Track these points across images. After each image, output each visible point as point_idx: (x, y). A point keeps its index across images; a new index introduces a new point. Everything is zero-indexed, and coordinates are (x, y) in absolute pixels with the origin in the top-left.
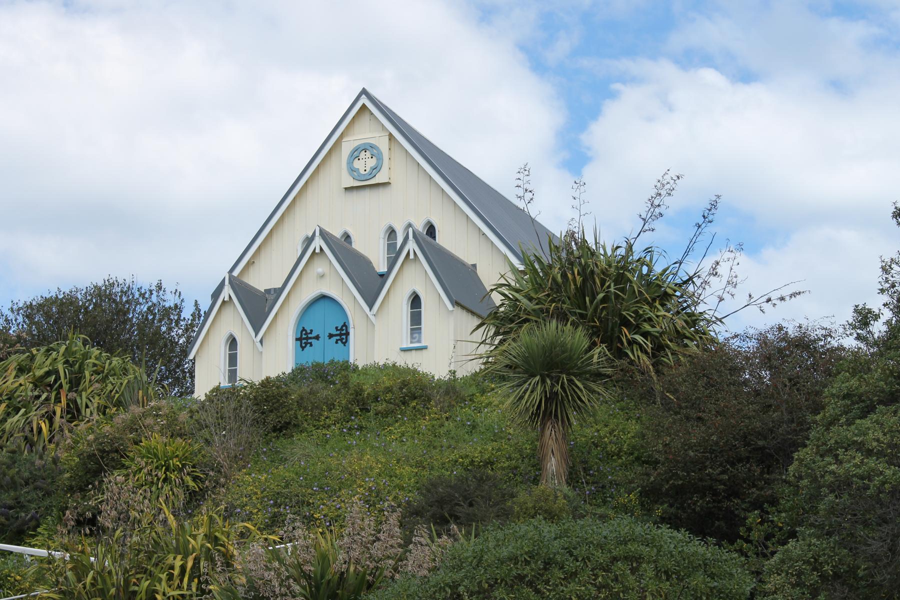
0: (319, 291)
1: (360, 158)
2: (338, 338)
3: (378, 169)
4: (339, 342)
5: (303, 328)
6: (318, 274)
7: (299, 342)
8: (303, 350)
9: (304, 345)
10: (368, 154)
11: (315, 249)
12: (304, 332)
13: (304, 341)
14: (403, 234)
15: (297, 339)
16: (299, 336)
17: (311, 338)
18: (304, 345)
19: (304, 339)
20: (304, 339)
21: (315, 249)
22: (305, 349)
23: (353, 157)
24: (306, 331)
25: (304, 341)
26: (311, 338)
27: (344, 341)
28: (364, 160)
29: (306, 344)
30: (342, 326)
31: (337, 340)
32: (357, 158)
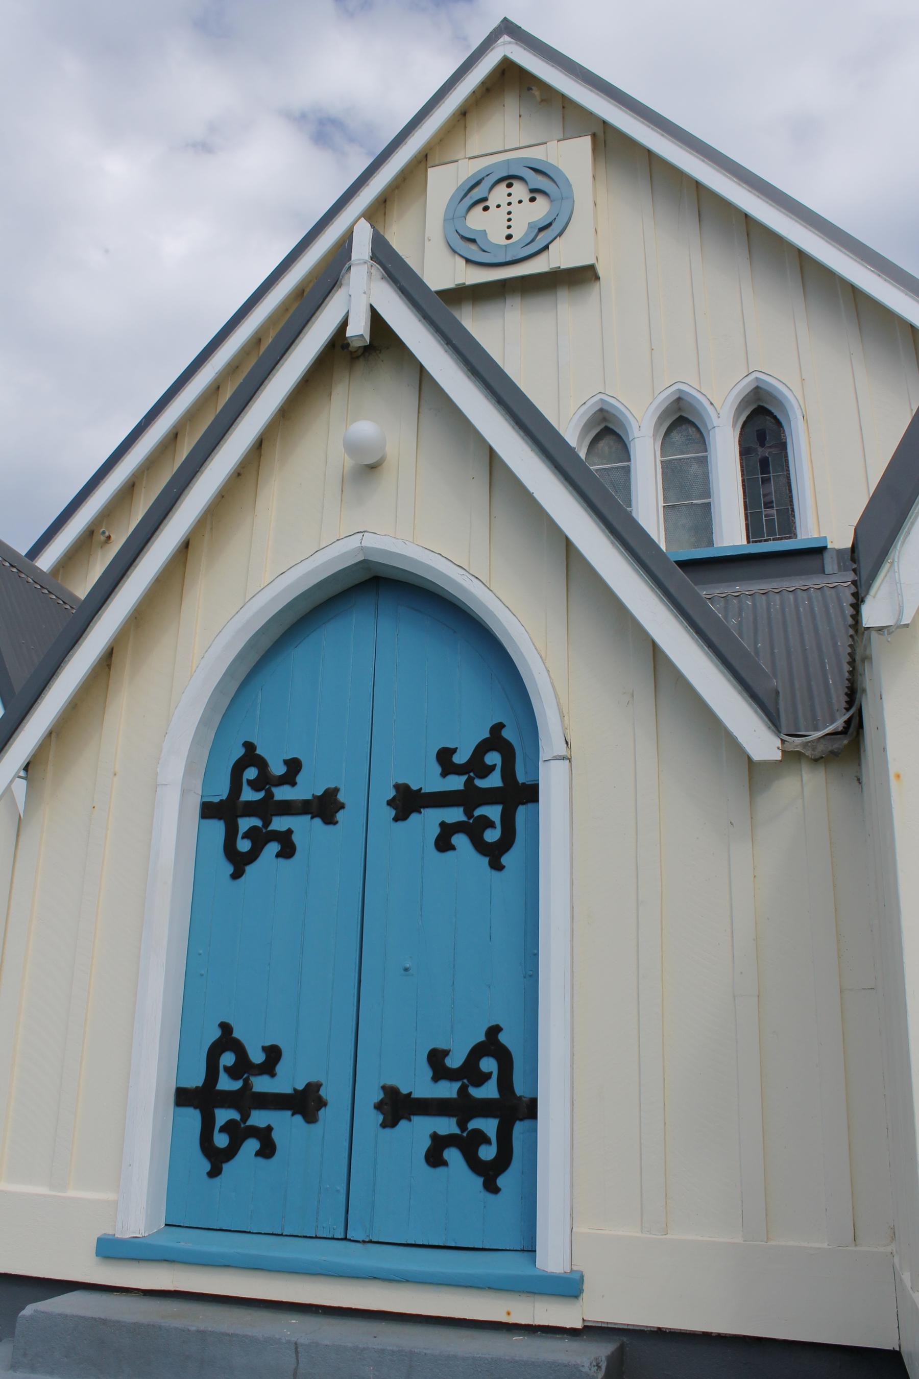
0: (354, 543)
1: (491, 203)
2: (447, 1126)
3: (556, 229)
4: (460, 840)
5: (249, 747)
6: (352, 448)
7: (218, 828)
8: (237, 874)
9: (221, 1140)
10: (519, 190)
11: (344, 324)
12: (251, 773)
13: (245, 824)
14: (734, 426)
15: (209, 811)
16: (196, 1080)
17: (287, 808)
18: (244, 846)
19: (250, 809)
20: (250, 809)
21: (344, 324)
22: (251, 870)
23: (468, 201)
24: (261, 764)
25: (223, 1116)
26: (287, 808)
27: (492, 836)
28: (505, 208)
29: (259, 838)
30: (483, 748)
31: (439, 1144)
32: (481, 207)
